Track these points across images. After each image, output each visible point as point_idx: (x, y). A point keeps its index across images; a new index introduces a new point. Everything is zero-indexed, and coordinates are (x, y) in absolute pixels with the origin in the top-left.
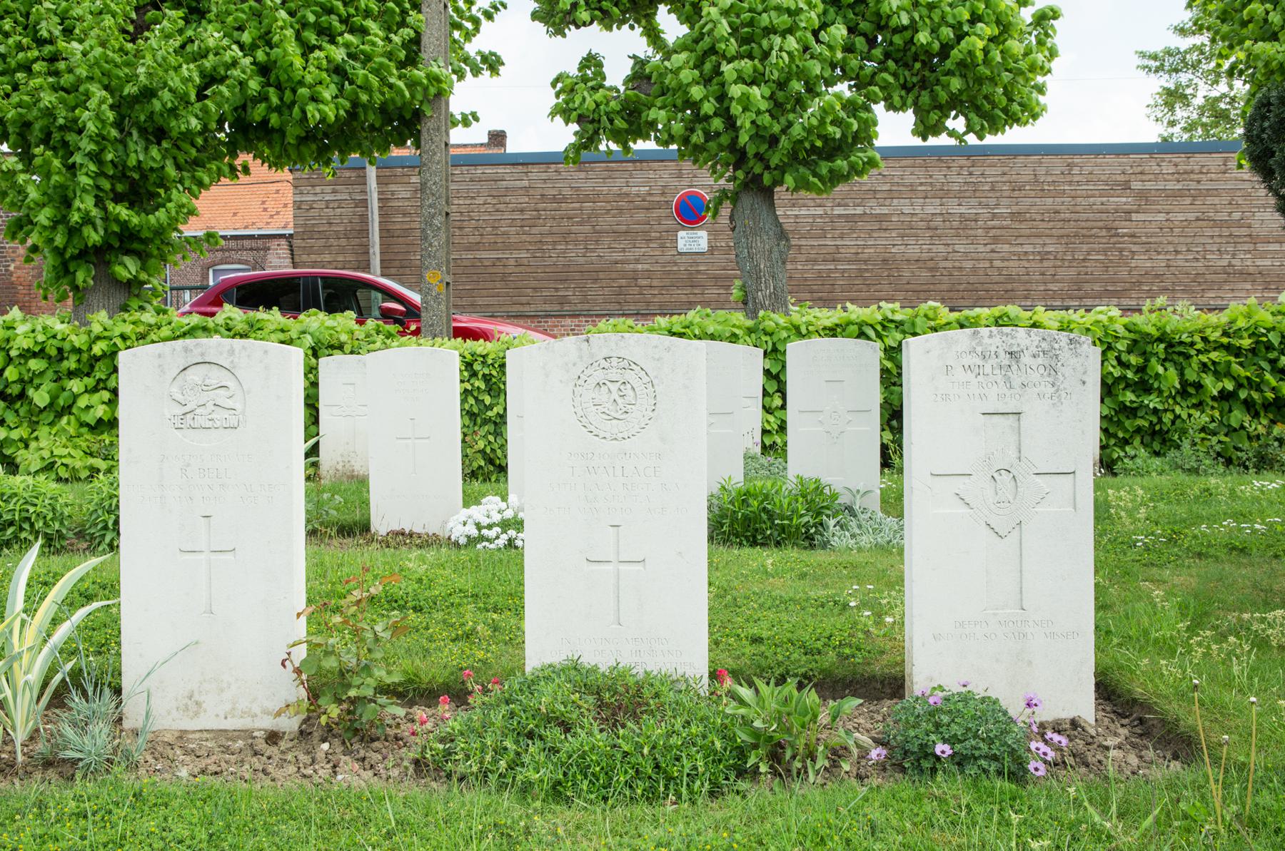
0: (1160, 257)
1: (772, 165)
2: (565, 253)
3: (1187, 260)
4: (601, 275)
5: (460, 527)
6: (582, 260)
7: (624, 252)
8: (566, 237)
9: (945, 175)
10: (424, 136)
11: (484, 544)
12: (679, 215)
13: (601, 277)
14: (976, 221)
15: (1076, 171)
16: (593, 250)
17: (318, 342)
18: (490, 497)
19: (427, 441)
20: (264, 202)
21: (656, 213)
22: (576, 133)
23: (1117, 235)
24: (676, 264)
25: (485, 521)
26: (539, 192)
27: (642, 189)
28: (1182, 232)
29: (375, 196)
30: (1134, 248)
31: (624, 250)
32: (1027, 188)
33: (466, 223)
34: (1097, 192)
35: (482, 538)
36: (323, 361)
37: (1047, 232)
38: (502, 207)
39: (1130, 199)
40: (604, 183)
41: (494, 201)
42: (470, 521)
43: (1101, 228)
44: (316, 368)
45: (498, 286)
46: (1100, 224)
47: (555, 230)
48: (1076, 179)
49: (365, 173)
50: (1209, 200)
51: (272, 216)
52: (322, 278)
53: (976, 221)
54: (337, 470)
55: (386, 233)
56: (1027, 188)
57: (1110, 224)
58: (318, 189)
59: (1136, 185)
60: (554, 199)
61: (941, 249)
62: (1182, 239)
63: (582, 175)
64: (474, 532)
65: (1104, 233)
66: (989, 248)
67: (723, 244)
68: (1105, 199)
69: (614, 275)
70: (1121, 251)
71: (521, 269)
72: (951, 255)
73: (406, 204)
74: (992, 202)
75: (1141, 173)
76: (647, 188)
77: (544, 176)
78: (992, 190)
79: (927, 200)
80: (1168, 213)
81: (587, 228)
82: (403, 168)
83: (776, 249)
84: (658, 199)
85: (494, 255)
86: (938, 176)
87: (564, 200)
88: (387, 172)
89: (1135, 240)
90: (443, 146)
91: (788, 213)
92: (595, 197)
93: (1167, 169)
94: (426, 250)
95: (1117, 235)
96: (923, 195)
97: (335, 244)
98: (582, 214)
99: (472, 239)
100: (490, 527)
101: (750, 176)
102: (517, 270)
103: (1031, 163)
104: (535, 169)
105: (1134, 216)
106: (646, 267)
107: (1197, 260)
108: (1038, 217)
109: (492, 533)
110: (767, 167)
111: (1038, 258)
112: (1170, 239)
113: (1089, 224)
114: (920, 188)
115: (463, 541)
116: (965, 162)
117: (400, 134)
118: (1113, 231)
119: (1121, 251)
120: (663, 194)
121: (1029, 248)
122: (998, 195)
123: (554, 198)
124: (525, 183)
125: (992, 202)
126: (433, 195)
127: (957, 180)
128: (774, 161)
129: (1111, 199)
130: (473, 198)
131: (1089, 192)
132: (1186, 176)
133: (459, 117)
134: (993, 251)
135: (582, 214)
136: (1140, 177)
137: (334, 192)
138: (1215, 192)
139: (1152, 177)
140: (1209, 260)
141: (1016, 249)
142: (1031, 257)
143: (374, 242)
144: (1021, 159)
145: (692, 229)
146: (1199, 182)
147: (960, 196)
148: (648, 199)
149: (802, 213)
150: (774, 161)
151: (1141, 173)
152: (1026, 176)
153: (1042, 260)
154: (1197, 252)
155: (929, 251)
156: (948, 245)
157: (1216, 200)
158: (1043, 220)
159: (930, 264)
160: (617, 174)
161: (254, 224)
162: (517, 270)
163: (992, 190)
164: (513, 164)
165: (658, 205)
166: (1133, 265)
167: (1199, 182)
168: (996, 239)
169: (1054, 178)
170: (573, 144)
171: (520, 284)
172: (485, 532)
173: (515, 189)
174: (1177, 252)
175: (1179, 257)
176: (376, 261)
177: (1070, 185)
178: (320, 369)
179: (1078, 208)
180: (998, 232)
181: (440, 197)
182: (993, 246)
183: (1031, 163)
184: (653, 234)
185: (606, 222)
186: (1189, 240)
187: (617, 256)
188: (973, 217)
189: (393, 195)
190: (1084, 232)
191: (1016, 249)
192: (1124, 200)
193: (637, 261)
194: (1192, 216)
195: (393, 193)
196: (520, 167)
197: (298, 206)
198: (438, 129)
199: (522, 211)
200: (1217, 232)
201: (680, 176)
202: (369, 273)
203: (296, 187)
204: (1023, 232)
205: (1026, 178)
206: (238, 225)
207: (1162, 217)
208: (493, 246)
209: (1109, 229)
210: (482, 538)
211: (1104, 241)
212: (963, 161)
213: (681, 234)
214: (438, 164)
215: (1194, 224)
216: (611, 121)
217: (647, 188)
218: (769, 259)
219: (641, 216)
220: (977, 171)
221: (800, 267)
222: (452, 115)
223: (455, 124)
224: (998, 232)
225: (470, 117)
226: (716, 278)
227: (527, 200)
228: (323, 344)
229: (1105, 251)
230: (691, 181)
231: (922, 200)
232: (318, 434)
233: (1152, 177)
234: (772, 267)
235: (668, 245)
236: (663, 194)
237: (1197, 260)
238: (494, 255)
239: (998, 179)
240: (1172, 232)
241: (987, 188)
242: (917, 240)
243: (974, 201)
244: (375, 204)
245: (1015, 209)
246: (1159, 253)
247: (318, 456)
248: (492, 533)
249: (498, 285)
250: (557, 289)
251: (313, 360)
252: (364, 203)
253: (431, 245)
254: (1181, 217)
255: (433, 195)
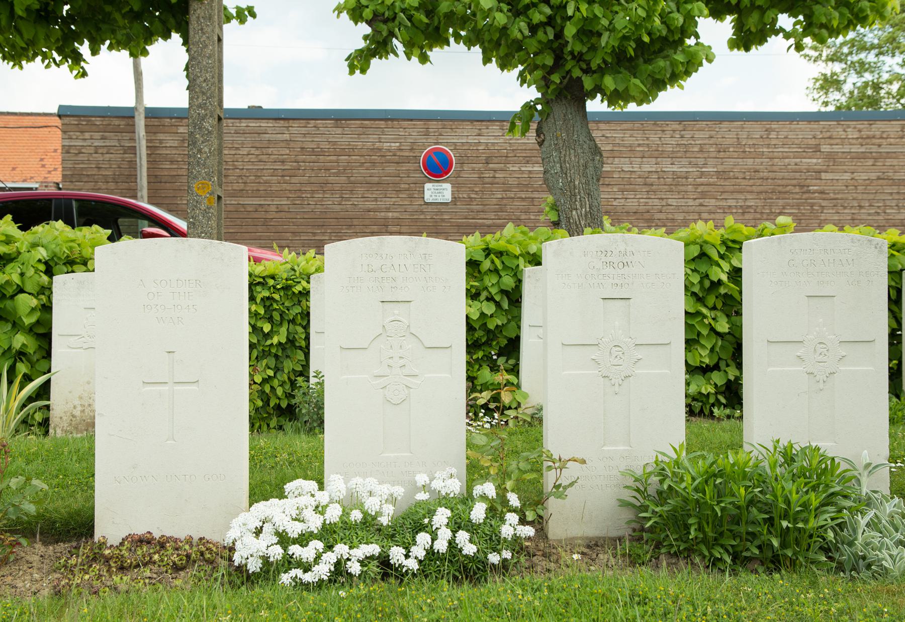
0: (846, 211)
1: (594, 66)
2: (322, 201)
3: (869, 214)
4: (355, 222)
5: (250, 538)
6: (338, 208)
7: (376, 201)
8: (324, 186)
9: (660, 138)
10: (193, 25)
11: (294, 572)
12: (425, 170)
13: (355, 223)
14: (687, 178)
15: (772, 136)
16: (348, 199)
17: (54, 255)
18: (299, 482)
19: (194, 387)
20: (42, 160)
21: (406, 166)
22: (366, 38)
23: (809, 192)
24: (422, 212)
25: (295, 530)
26: (299, 145)
27: (393, 144)
28: (865, 189)
29: (144, 143)
30: (824, 203)
31: (376, 199)
32: (731, 150)
33: (231, 171)
34: (791, 154)
35: (289, 562)
36: (59, 280)
37: (748, 188)
38: (264, 157)
39: (820, 161)
40: (359, 138)
41: (257, 152)
42: (268, 528)
43: (795, 186)
44: (50, 289)
45: (260, 230)
46: (794, 182)
47: (313, 180)
48: (773, 142)
49: (134, 122)
50: (889, 162)
51: (49, 172)
52: (76, 200)
53: (687, 178)
54: (73, 416)
55: (153, 160)
56: (731, 150)
57: (802, 182)
58: (87, 135)
59: (825, 148)
60: (313, 152)
61: (656, 202)
62: (865, 196)
63: (339, 131)
64: (277, 552)
65: (797, 190)
66: (698, 202)
67: (465, 196)
68: (798, 160)
69: (367, 222)
70: (812, 205)
71: (283, 215)
72: (665, 208)
73: (174, 152)
74: (701, 161)
75: (830, 138)
76: (398, 144)
77: (303, 130)
78: (701, 151)
79: (644, 160)
80: (853, 173)
81: (343, 179)
82: (171, 118)
83: (590, 164)
84: (407, 154)
85: (257, 201)
86: (654, 138)
87: (322, 153)
88: (156, 122)
89: (824, 196)
90: (216, 39)
91: (523, 169)
92: (350, 151)
93: (852, 134)
94: (195, 157)
95: (809, 192)
96: (640, 155)
97: (104, 187)
98: (339, 166)
99: (236, 186)
100: (303, 540)
101: (566, 81)
102: (277, 216)
103: (734, 128)
104: (296, 124)
105: (823, 175)
106: (396, 215)
107: (878, 213)
108: (741, 176)
109: (306, 553)
110: (587, 71)
111: (740, 211)
112: (855, 195)
113: (784, 182)
114: (638, 149)
115: (254, 566)
116: (677, 126)
117: (163, 22)
118: (806, 188)
119: (812, 205)
120: (412, 150)
121: (732, 203)
122: (706, 155)
123: (313, 151)
124: (286, 136)
125: (701, 161)
126: (203, 93)
127: (670, 142)
128: (596, 62)
129: (804, 160)
130: (237, 149)
131: (785, 154)
132: (868, 141)
133: (233, 12)
134: (701, 205)
135: (339, 166)
136: (829, 141)
137: (103, 138)
138: (894, 155)
139: (838, 141)
140: (889, 214)
141: (721, 203)
142: (734, 211)
143: (142, 186)
144: (725, 125)
145: (438, 181)
146: (879, 146)
147: (673, 156)
148: (398, 154)
149: (535, 169)
150: (596, 62)
151: (830, 138)
152: (730, 139)
153: (743, 213)
154: (879, 207)
155: (646, 204)
156: (662, 199)
157: (895, 162)
158: (744, 178)
159: (647, 216)
160: (371, 131)
161: (32, 178)
162: (277, 216)
163: (701, 151)
164: (276, 119)
165: (407, 160)
166: (822, 218)
167: (879, 146)
168: (704, 195)
169: (754, 142)
170: (361, 51)
171: (280, 228)
172: (295, 549)
173: (276, 142)
174: (861, 207)
175: (863, 211)
176: (144, 192)
177: (768, 148)
178: (54, 290)
179: (775, 168)
180: (706, 188)
181: (212, 97)
182: (701, 201)
183: (734, 128)
184: (403, 186)
185: (359, 174)
186: (871, 196)
187: (370, 205)
188: (684, 174)
189: (161, 143)
190: (780, 188)
191: (721, 203)
192: (814, 161)
193: (388, 210)
194: (873, 176)
195: (161, 141)
196: (282, 122)
197: (66, 150)
198: (210, 18)
199: (283, 162)
200: (895, 189)
201: (427, 134)
202: (135, 197)
203: (64, 132)
204: (727, 188)
205: (729, 141)
206: (17, 179)
207: (847, 176)
208: (256, 194)
209: (802, 186)
210: (289, 562)
211: (798, 196)
212: (676, 126)
213: (428, 186)
214: (209, 58)
215: (875, 183)
216: (410, 18)
217: (398, 144)
218: (585, 175)
219: (391, 169)
220: (688, 134)
221: (532, 217)
222: (225, 8)
223: (228, 19)
224: (706, 188)
225: (246, 13)
226: (459, 226)
227: (288, 152)
228: (59, 258)
229: (798, 206)
230: (437, 139)
231: (640, 160)
232: (49, 371)
233: (838, 141)
234: (587, 183)
235: (416, 196)
236: (412, 150)
237: (878, 213)
238: (257, 201)
239: (706, 142)
240: (856, 189)
241: (696, 149)
242: (636, 195)
243: (685, 161)
244: (143, 151)
245: (720, 168)
246: (845, 208)
247: (49, 399)
248: (306, 553)
249: (260, 229)
250: (314, 234)
251: (45, 278)
252: (133, 150)
253: (200, 151)
254: (864, 176)
255: (203, 93)
